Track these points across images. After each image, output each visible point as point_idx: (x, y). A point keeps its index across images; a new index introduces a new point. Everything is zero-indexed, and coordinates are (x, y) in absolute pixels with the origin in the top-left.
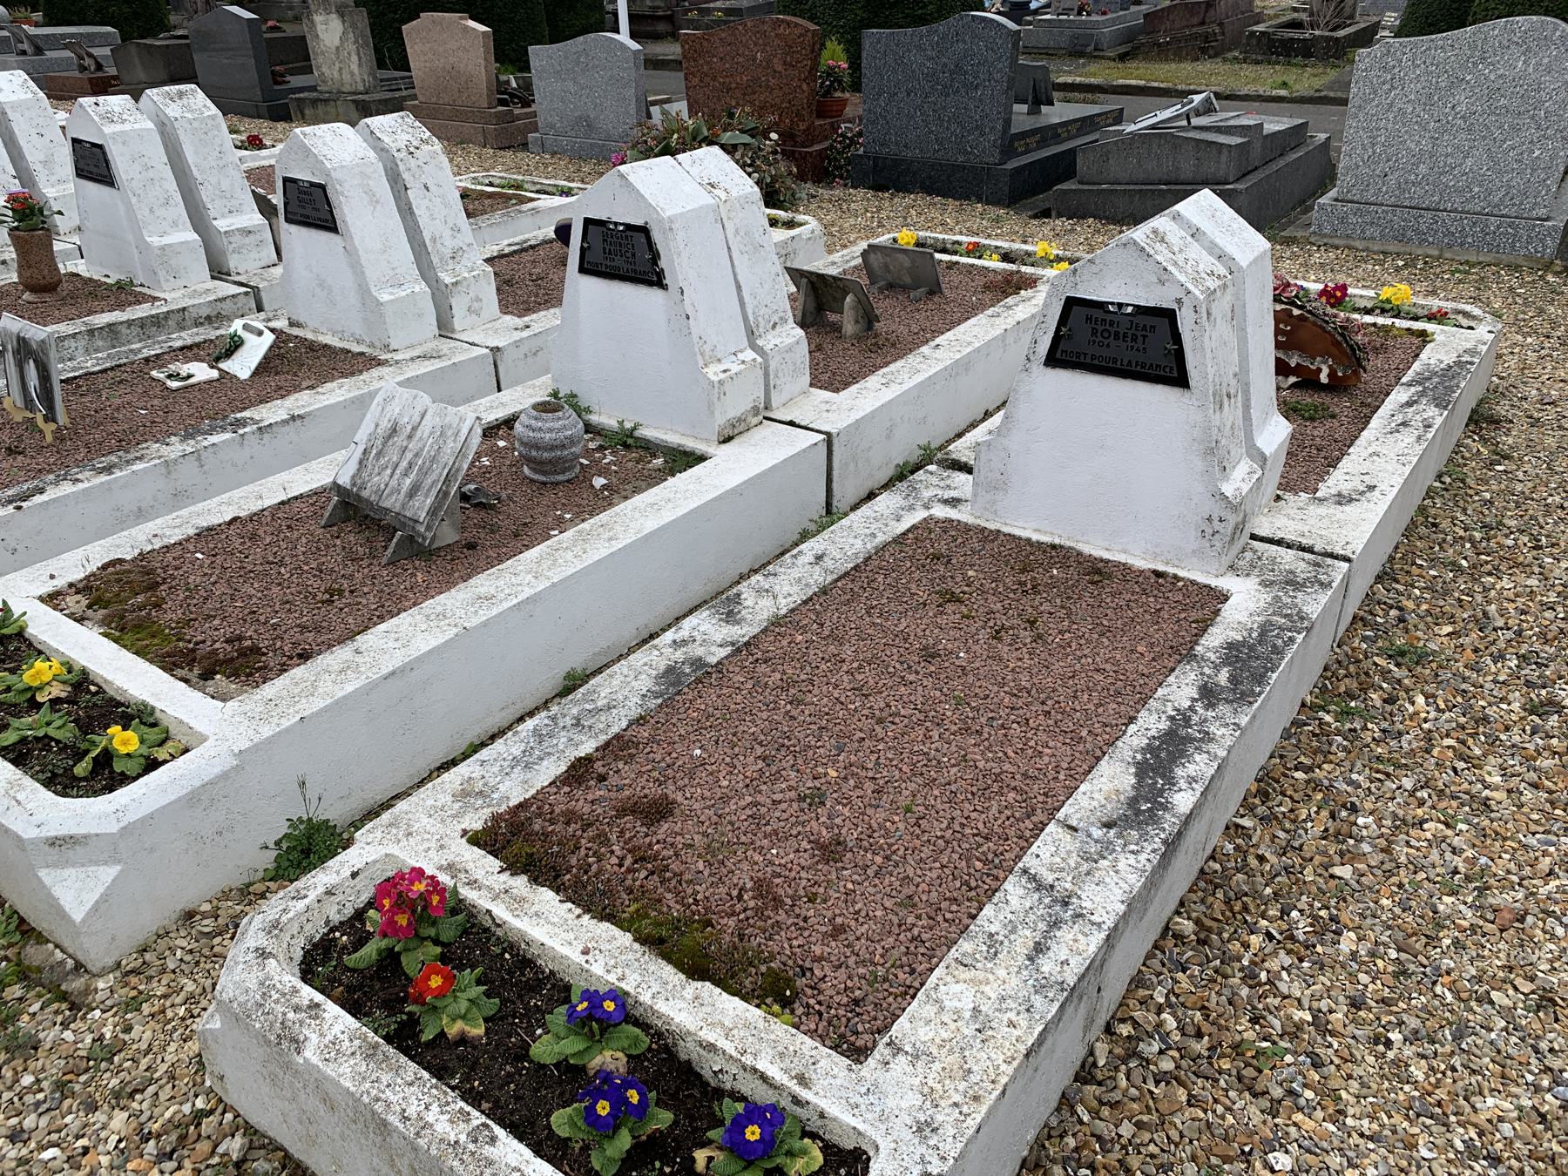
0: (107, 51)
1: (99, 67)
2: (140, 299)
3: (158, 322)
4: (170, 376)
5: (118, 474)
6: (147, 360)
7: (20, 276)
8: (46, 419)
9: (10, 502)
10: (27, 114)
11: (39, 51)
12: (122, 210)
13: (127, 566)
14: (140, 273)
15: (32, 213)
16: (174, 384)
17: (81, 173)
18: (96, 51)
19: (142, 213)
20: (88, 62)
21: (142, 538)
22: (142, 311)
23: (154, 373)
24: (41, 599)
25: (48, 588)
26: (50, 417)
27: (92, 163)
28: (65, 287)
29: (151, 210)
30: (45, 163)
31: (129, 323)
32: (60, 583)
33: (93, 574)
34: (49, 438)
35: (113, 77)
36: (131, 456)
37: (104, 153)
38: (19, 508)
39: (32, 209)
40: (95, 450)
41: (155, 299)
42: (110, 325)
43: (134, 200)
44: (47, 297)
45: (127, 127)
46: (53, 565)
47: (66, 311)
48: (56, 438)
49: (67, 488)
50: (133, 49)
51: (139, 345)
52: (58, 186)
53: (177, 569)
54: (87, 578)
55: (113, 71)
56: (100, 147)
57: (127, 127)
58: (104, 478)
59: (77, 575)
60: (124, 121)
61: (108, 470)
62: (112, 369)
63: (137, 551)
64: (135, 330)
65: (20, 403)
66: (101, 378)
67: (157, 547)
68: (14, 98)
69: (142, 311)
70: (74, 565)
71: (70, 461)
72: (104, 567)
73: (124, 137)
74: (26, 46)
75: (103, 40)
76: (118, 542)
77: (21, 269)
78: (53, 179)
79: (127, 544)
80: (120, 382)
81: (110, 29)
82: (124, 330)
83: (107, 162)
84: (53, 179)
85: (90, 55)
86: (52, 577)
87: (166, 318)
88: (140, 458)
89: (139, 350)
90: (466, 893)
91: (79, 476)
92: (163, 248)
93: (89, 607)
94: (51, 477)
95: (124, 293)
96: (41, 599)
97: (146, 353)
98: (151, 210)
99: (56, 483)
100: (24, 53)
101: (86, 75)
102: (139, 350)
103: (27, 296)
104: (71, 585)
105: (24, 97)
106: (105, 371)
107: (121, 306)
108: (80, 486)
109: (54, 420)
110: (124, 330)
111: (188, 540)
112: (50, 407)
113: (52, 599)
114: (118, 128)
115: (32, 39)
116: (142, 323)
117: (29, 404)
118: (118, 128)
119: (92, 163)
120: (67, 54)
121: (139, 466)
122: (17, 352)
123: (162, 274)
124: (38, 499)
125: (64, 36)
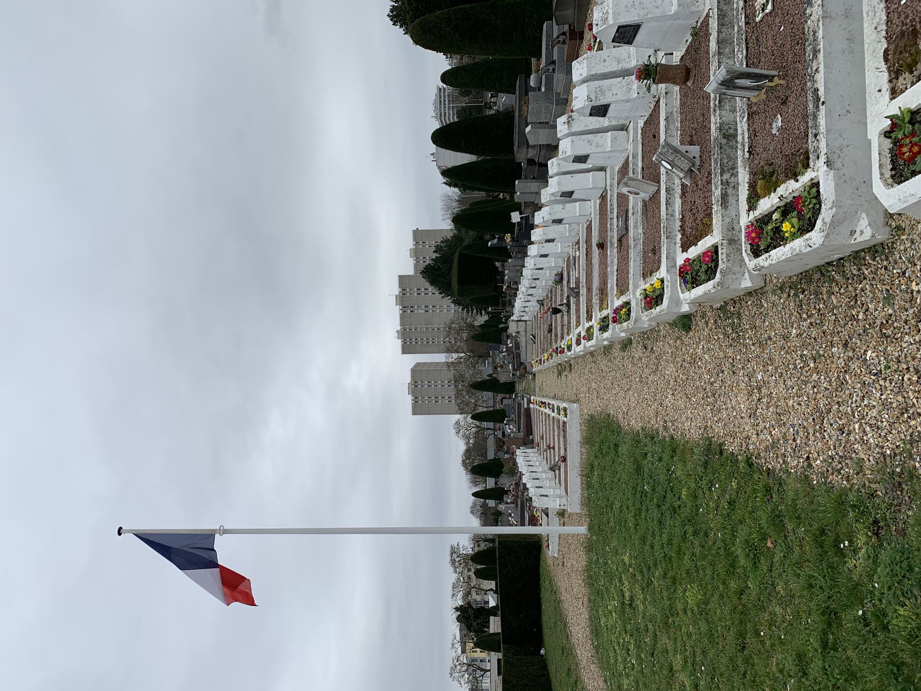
0: (556, 27)
1: (564, 34)
2: (706, 23)
3: (722, 16)
4: (763, 10)
5: (821, 47)
6: (747, 23)
7: (677, 84)
8: (771, 81)
9: (818, 107)
10: (594, 65)
11: (553, 62)
12: (653, 24)
13: (892, 47)
14: (690, 22)
15: (648, 70)
16: (769, 7)
17: (630, 42)
18: (555, 35)
19: (658, 12)
20: (561, 39)
21: (874, 36)
22: (714, 24)
23: (758, 19)
24: (891, 99)
25: (886, 95)
26: (771, 78)
27: (626, 34)
28: (689, 64)
29: (657, 7)
30: (619, 62)
31: (719, 32)
32: (886, 87)
33: (888, 68)
34: (782, 82)
35: (570, 27)
36: (811, 38)
37: (623, 27)
38: (823, 103)
39: (645, 70)
40: (800, 58)
41: (708, 15)
42: (718, 42)
43: (650, 16)
44: (692, 74)
45: (610, 11)
46: (871, 90)
47: (703, 66)
48: (784, 79)
49: (820, 77)
50: (557, 13)
51: (736, 28)
52: (632, 56)
53: (907, 17)
54: (889, 71)
55: (566, 28)
56: (619, 27)
57: (610, 11)
58: (821, 56)
59: (886, 76)
60: (607, 12)
61: (816, 52)
62: (747, 44)
63: (884, 40)
64: (724, 29)
65: (756, 93)
66: (751, 50)
67: (885, 28)
68: (585, 69)
69: (714, 24)
70: (876, 75)
71: (802, 73)
72: (886, 60)
73: (616, 14)
74: (551, 68)
75: (550, 29)
76: (870, 51)
77: (674, 83)
78: (627, 60)
79: (874, 45)
80: (757, 40)
81: (545, 26)
82: (723, 35)
83: (627, 26)
84: (627, 60)
85: (558, 37)
86: (880, 91)
87: (722, 11)
88: (815, 32)
89: (739, 27)
90: (458, 638)
91: (814, 69)
92: (679, 5)
93: (911, 72)
94: (809, 84)
95: (700, 34)
96: (891, 99)
97: (742, 23)
98: (657, 7)
99: (814, 81)
100: (554, 70)
101: (567, 41)
102: (739, 27)
103: (689, 84)
104: (890, 81)
105: (585, 64)
106: (747, 48)
107: (707, 35)
108: (821, 68)
109: (773, 77)
110: (723, 35)
111: (887, 8)
112: (765, 77)
113: (895, 93)
114: (610, 16)
115: (547, 64)
116: (721, 25)
117: (758, 88)
118: (610, 16)
119: (626, 34)
120: (556, 49)
121: (820, 34)
122: (728, 88)
123: (694, 9)
124: (821, 93)
125: (547, 49)
